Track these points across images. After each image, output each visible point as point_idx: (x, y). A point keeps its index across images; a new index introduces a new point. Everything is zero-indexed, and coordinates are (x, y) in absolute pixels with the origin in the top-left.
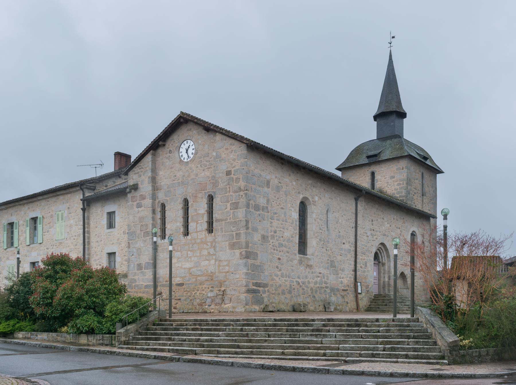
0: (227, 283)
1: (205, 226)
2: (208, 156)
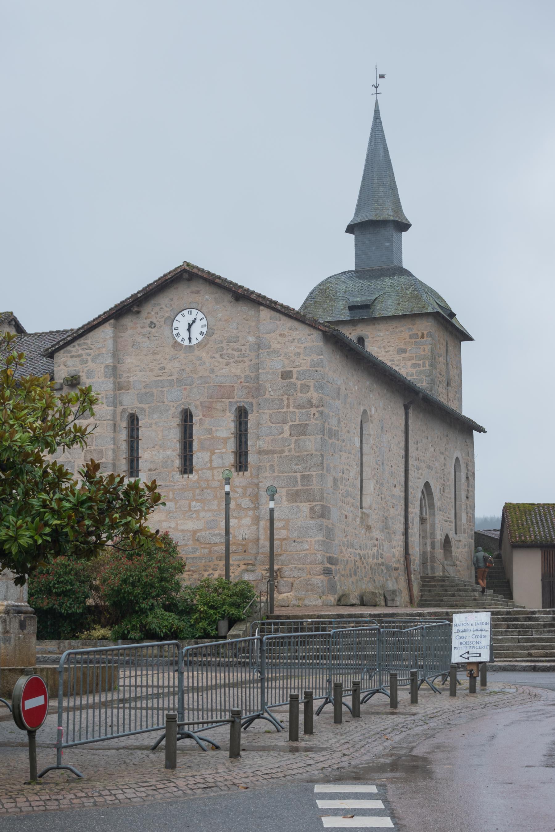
0: (283, 558)
1: (231, 459)
2: (238, 341)
